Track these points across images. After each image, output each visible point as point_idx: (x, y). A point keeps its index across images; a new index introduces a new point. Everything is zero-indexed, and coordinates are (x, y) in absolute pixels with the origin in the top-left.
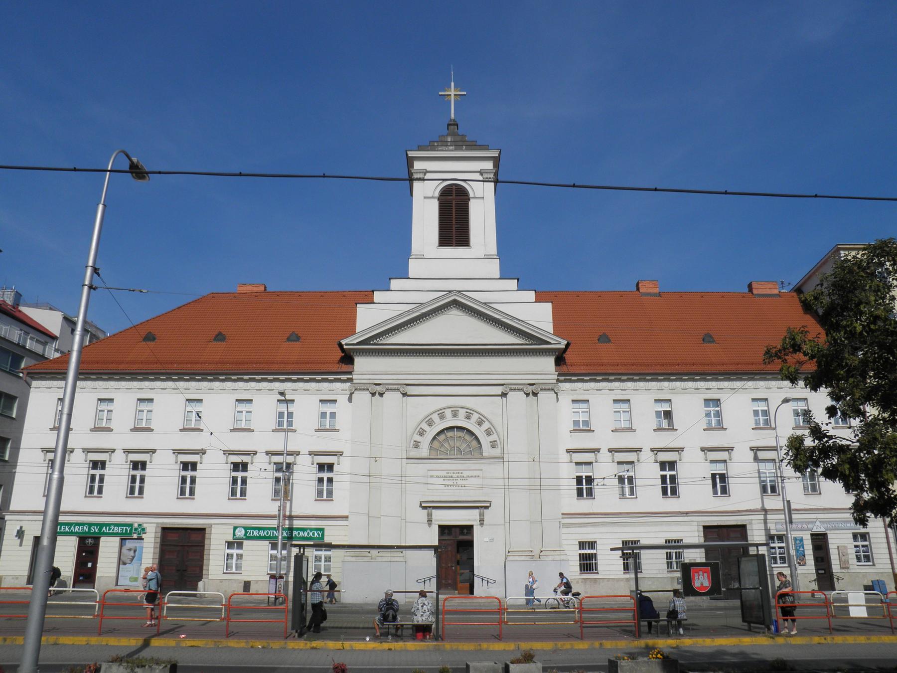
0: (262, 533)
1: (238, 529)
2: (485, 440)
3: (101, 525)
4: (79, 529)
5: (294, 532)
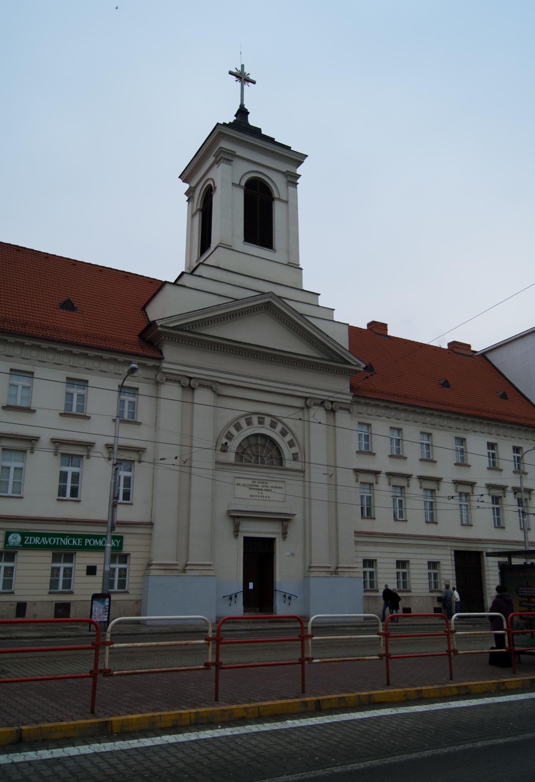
0: (45, 541)
1: (13, 535)
2: (287, 452)
4: (77, 542)
5: (86, 540)
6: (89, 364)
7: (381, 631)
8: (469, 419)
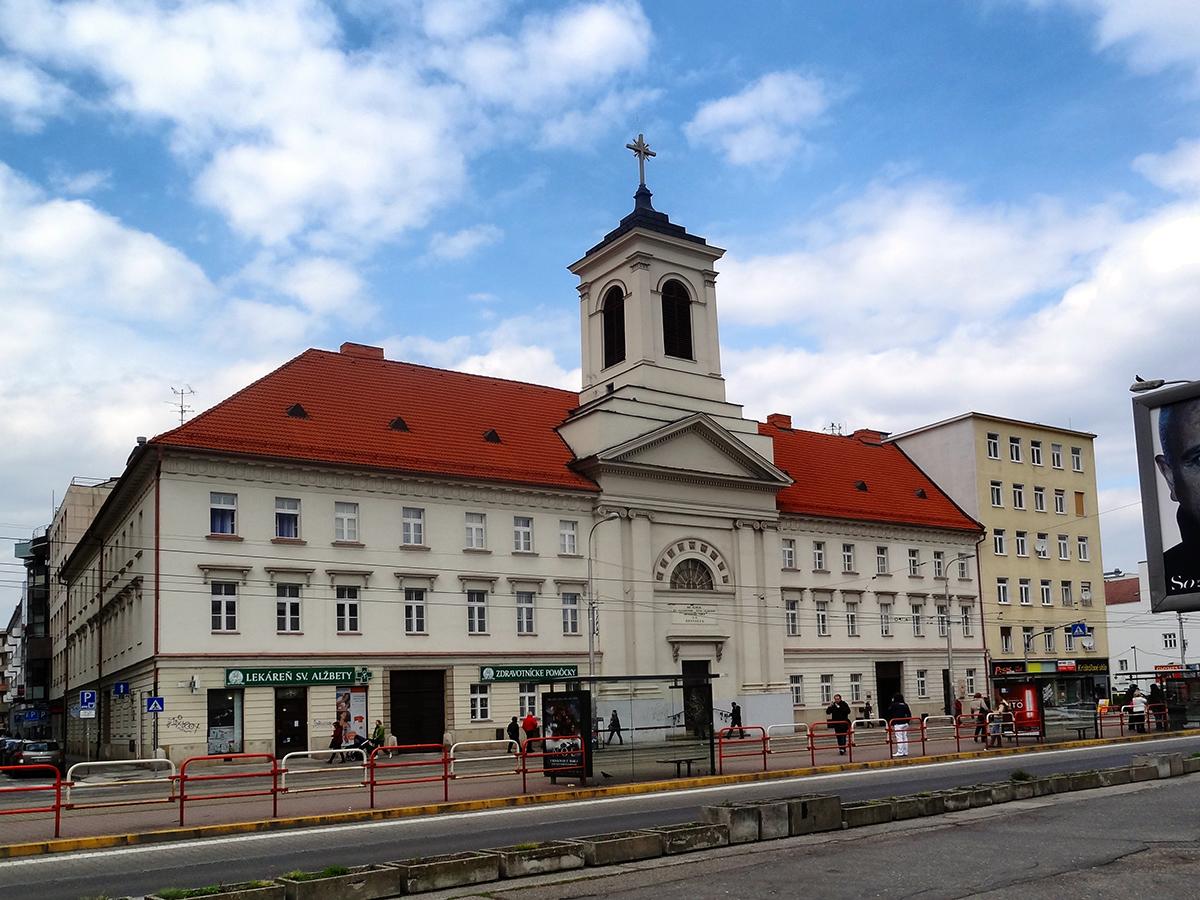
3: (310, 671)
4: (278, 677)
6: (533, 501)
7: (365, 762)
8: (891, 527)
